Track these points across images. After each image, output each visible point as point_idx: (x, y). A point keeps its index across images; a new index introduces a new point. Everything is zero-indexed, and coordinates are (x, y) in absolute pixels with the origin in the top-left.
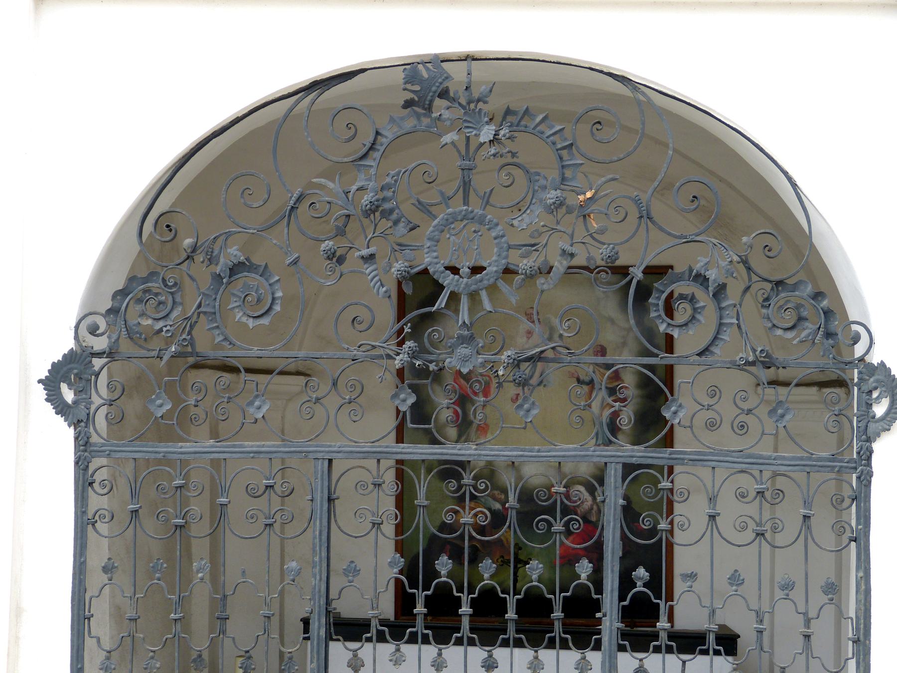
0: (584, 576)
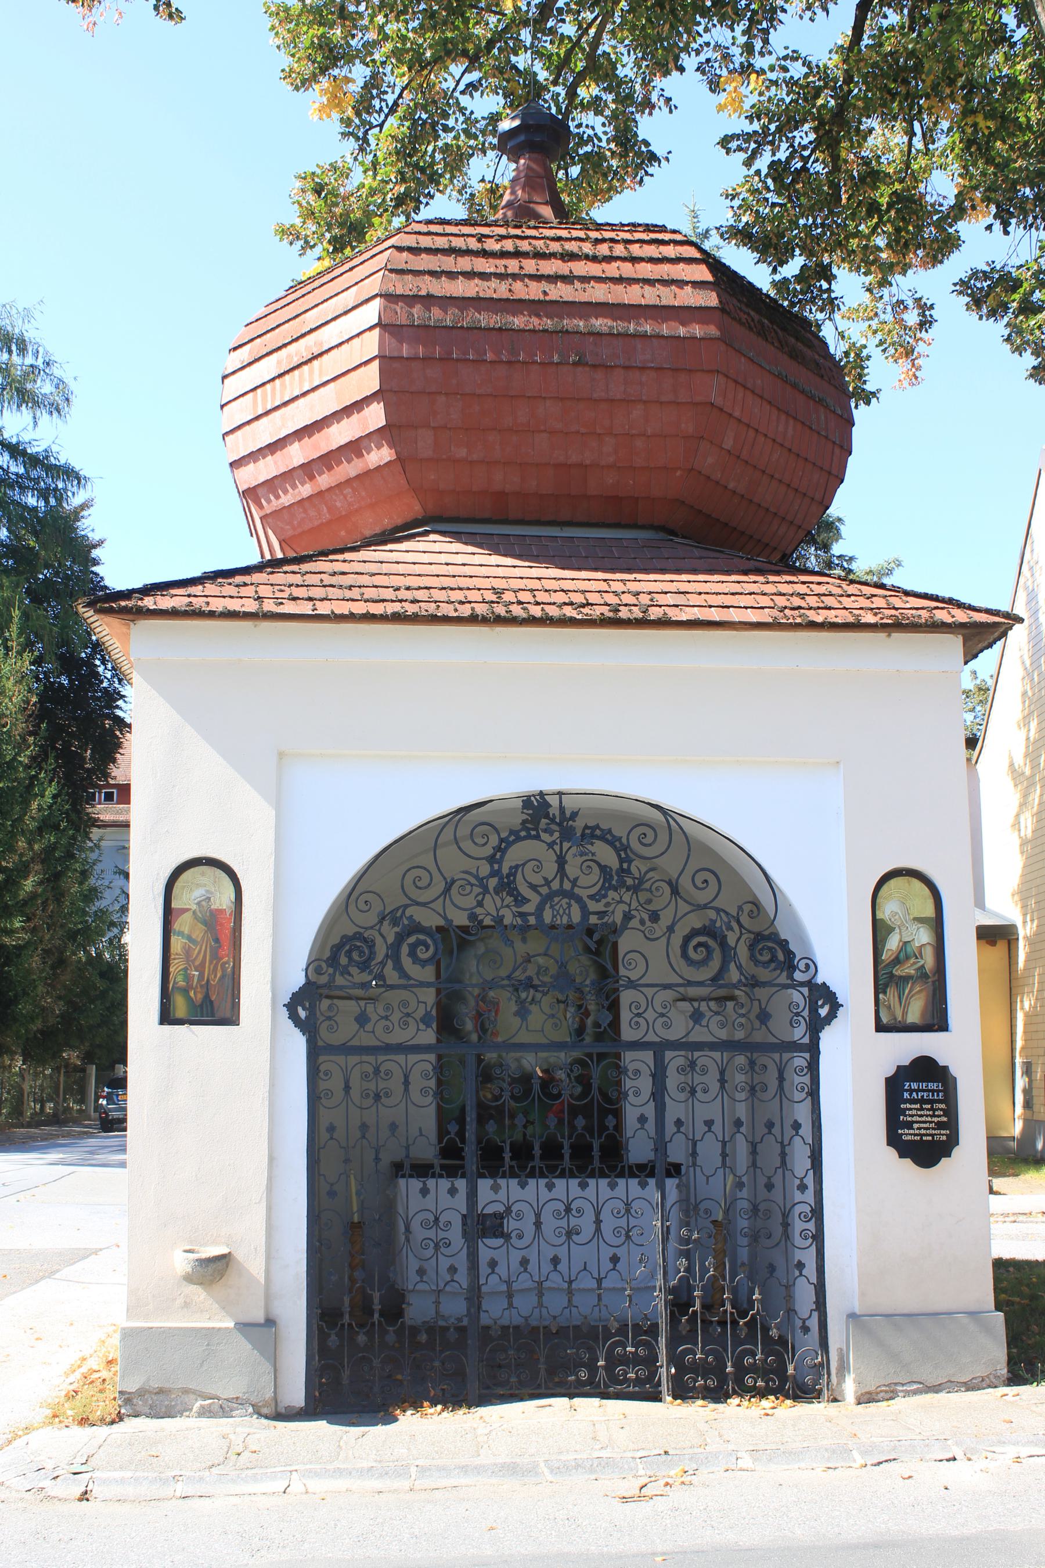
0: (552, 1127)
